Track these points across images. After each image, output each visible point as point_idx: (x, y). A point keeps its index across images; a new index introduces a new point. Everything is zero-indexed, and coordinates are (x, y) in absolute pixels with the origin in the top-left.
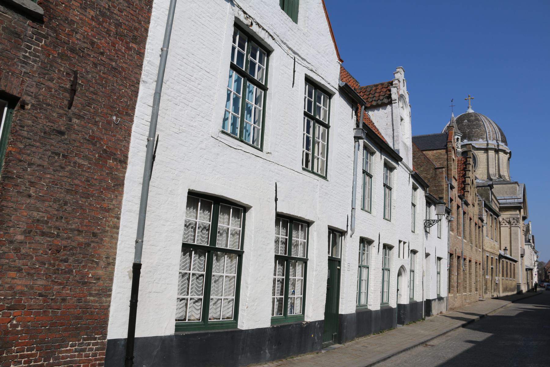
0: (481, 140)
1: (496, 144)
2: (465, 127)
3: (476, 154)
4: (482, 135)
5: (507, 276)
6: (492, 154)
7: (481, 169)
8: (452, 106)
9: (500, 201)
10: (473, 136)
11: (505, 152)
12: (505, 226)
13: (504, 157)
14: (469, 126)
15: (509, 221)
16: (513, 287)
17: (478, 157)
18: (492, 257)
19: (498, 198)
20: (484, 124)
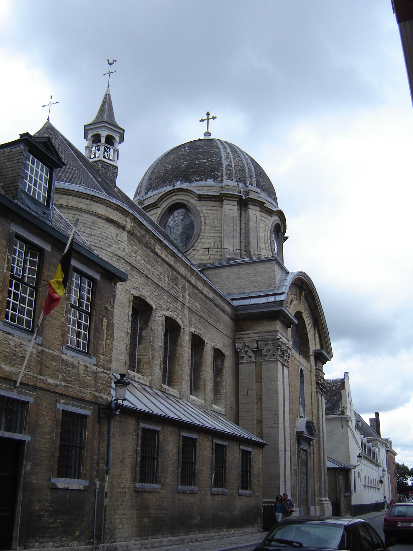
0: (210, 182)
3: (198, 208)
4: (213, 171)
8: (110, 73)
9: (235, 303)
12: (249, 360)
13: (263, 219)
16: (237, 512)
17: (202, 215)
19: (229, 298)
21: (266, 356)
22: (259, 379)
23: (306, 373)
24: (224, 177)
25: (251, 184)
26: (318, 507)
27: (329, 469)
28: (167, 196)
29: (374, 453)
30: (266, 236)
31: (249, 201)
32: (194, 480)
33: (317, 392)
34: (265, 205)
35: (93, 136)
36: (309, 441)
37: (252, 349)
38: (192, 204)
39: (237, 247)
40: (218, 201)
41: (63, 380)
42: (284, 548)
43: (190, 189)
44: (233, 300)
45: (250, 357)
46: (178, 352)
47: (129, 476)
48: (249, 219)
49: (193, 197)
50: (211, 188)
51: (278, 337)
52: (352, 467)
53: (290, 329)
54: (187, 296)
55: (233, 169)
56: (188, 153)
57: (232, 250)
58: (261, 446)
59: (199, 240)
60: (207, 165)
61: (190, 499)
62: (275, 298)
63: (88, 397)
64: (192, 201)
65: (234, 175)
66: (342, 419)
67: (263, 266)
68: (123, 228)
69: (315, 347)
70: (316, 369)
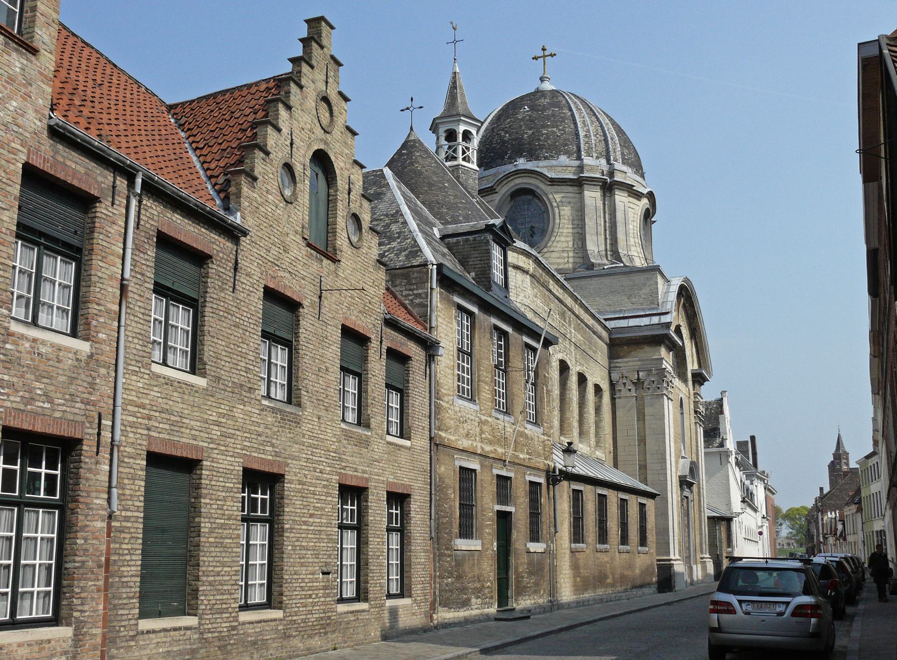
0: (563, 159)
1: (605, 168)
2: (522, 123)
4: (566, 145)
5: (603, 537)
6: (593, 194)
7: (563, 239)
8: (455, 42)
9: (611, 325)
10: (542, 147)
11: (630, 189)
13: (632, 206)
14: (531, 121)
15: (638, 379)
16: (637, 571)
18: (504, 473)
20: (573, 115)
21: (649, 388)
22: (641, 416)
23: (685, 401)
24: (583, 153)
25: (616, 160)
26: (699, 566)
27: (709, 518)
28: (507, 178)
29: (752, 493)
30: (635, 228)
31: (615, 184)
32: (607, 539)
33: (696, 423)
34: (634, 188)
35: (446, 131)
36: (690, 485)
37: (631, 381)
38: (541, 190)
39: (602, 248)
40: (576, 186)
41: (528, 453)
42: (638, 614)
43: (538, 170)
44: (606, 320)
45: (630, 390)
46: (568, 396)
47: (567, 542)
48: (615, 209)
49: (544, 180)
50: (566, 168)
51: (664, 367)
52: (734, 515)
53: (671, 353)
54: (573, 331)
55: (593, 142)
56: (530, 116)
57: (596, 252)
58: (652, 496)
59: (553, 239)
60: (557, 136)
61: (604, 558)
62: (660, 319)
63: (541, 466)
64: (542, 187)
65: (594, 150)
66: (720, 453)
67: (643, 277)
68: (526, 272)
69: (693, 365)
70: (694, 394)
